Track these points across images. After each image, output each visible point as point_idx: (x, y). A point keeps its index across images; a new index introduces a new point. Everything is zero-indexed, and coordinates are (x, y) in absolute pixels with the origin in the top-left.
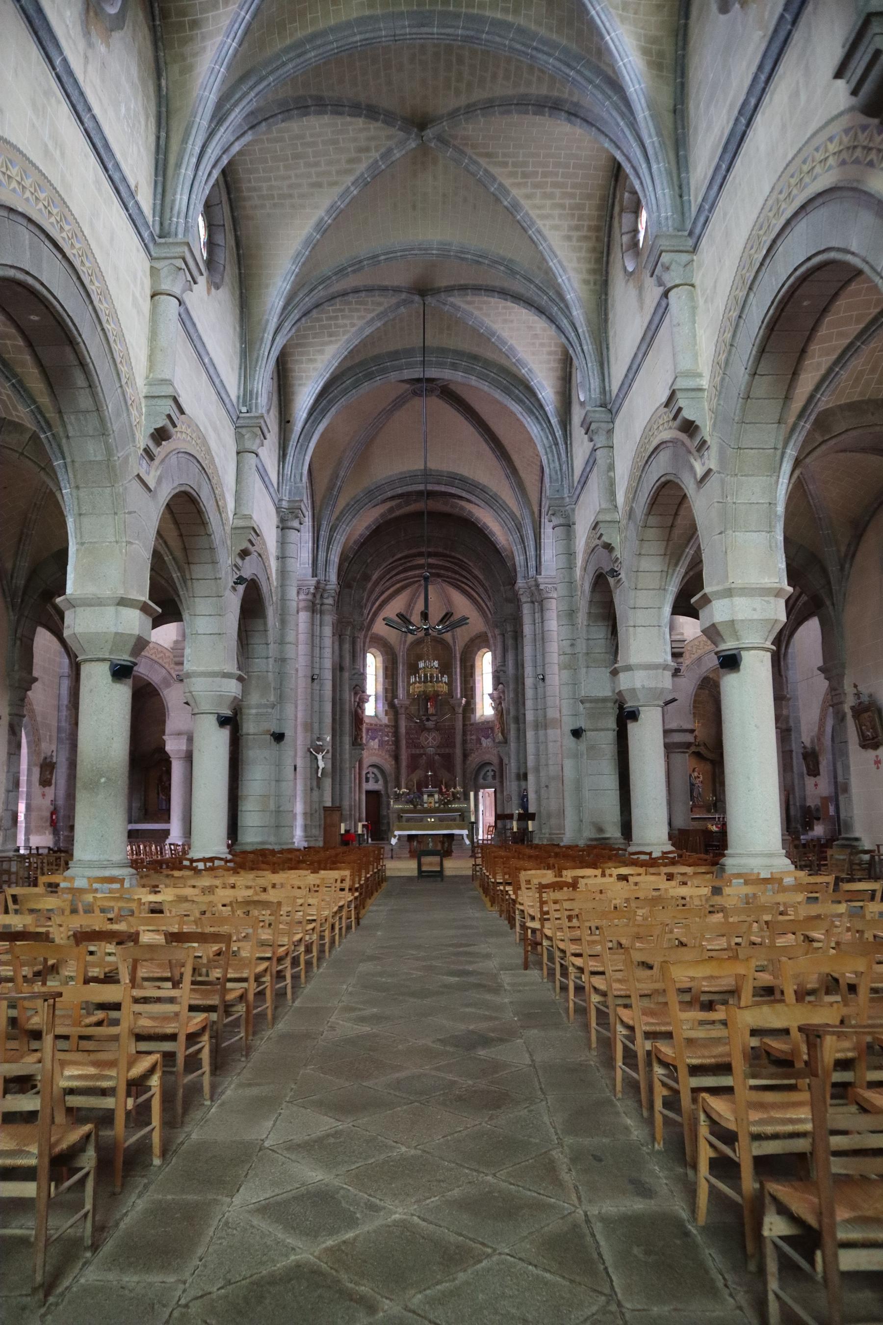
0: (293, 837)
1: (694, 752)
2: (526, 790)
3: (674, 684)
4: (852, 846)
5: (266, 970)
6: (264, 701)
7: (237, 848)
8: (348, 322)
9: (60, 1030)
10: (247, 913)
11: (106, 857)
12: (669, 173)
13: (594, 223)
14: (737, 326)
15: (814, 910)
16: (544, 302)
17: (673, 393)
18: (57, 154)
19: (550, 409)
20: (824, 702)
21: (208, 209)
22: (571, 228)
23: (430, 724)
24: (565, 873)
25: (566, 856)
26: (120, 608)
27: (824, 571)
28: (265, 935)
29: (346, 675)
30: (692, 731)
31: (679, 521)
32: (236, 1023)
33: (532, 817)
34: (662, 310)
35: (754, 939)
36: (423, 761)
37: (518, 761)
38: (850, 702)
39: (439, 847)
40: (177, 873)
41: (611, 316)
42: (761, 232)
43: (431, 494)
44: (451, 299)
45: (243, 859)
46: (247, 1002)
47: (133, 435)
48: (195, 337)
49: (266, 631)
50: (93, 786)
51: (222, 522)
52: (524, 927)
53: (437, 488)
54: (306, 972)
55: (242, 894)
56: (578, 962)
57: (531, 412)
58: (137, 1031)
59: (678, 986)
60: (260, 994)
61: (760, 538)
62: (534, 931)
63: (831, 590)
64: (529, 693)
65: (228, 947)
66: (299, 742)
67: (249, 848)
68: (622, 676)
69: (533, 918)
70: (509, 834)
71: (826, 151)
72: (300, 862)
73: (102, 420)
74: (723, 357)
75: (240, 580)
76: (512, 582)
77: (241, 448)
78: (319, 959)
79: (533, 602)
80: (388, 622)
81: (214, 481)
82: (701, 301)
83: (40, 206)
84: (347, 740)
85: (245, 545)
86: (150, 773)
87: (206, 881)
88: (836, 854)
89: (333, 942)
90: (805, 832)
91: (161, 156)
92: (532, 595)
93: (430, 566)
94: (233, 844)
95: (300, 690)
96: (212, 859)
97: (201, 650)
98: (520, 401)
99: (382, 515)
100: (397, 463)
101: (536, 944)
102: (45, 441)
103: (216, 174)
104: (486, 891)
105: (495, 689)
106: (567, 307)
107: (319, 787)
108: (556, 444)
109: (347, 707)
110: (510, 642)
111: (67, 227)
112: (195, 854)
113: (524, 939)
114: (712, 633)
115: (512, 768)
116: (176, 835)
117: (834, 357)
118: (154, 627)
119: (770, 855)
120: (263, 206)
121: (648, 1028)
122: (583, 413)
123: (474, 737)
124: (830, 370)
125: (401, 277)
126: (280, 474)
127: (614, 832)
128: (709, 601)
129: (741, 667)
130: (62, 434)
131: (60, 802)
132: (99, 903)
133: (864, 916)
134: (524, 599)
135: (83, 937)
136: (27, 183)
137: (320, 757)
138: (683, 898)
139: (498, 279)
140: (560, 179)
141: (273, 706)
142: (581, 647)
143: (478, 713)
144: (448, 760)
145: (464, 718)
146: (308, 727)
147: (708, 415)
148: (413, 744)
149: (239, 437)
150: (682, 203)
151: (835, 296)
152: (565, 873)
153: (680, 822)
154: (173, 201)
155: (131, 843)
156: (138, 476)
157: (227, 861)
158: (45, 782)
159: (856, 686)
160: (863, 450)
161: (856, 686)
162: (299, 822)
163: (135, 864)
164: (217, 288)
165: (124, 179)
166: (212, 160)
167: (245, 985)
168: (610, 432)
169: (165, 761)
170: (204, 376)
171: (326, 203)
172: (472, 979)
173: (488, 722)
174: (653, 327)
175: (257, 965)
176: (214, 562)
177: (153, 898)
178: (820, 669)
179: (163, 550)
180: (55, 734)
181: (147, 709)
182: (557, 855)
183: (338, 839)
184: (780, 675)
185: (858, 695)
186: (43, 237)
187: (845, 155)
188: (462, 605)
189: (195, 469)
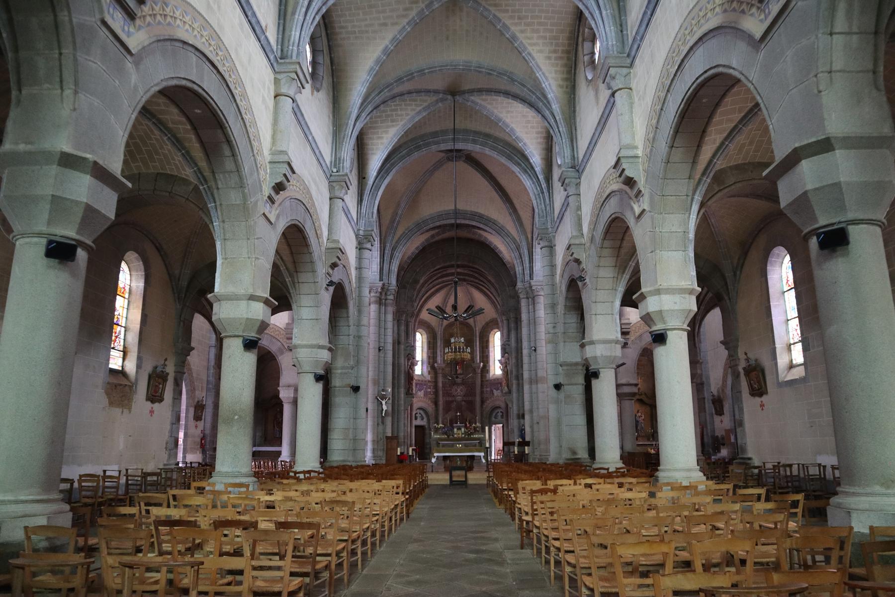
0: (365, 457)
1: (638, 400)
2: (524, 425)
3: (623, 354)
4: (746, 463)
5: (344, 548)
6: (346, 364)
7: (327, 464)
8: (404, 113)
9: (201, 588)
10: (332, 509)
11: (237, 469)
12: (614, 17)
13: (566, 48)
14: (660, 115)
15: (719, 508)
16: (533, 99)
17: (619, 159)
18: (215, 7)
19: (538, 169)
20: (726, 365)
21: (313, 41)
22: (550, 52)
23: (459, 381)
24: (549, 482)
25: (550, 471)
26: (250, 302)
27: (723, 277)
28: (344, 524)
29: (402, 347)
30: (636, 385)
31: (625, 244)
32: (322, 585)
33: (528, 444)
34: (611, 104)
35: (677, 528)
36: (454, 405)
37: (518, 406)
38: (742, 365)
39: (464, 465)
40: (285, 481)
41: (577, 108)
42: (674, 55)
43: (459, 226)
44: (472, 98)
45: (331, 471)
46: (330, 570)
47: (261, 187)
48: (303, 123)
49: (348, 317)
50: (229, 421)
51: (319, 244)
52: (521, 520)
53: (463, 222)
54: (372, 550)
55: (329, 496)
56: (557, 544)
57: (525, 171)
58: (255, 589)
59: (622, 560)
60: (340, 565)
61: (679, 255)
62: (528, 522)
63: (728, 289)
64: (526, 360)
65: (318, 531)
66: (370, 392)
67: (335, 464)
68: (587, 348)
69: (527, 514)
70: (512, 455)
71: (706, 8)
72: (369, 474)
73: (240, 177)
74: (651, 136)
75: (331, 283)
76: (514, 284)
77: (332, 196)
78: (380, 541)
79: (528, 298)
80: (430, 312)
81: (314, 217)
82: (636, 100)
83: (204, 40)
84: (402, 390)
85: (335, 260)
86: (268, 412)
87: (304, 487)
88: (735, 469)
89: (390, 529)
90: (715, 454)
91: (283, 7)
92: (527, 293)
93: (459, 274)
94: (324, 461)
95: (371, 357)
96: (309, 472)
97: (303, 330)
98: (518, 165)
99: (427, 240)
100: (436, 206)
101: (529, 531)
102: (203, 192)
103: (318, 18)
104: (496, 495)
105: (502, 357)
106: (548, 102)
107: (383, 423)
108: (543, 193)
109: (403, 368)
110: (512, 325)
111: (220, 53)
112: (298, 468)
113: (521, 527)
114: (647, 319)
115: (514, 410)
116: (285, 456)
117: (725, 135)
118: (272, 315)
119: (689, 470)
120: (349, 38)
121: (603, 590)
122: (560, 172)
124: (722, 144)
125: (439, 84)
126: (359, 212)
127: (583, 455)
128: (645, 298)
129: (668, 342)
130: (214, 186)
131: (208, 432)
132: (231, 501)
133: (752, 512)
134: (521, 296)
135: (220, 524)
136: (196, 25)
137: (384, 402)
138: (630, 500)
139: (503, 85)
140: (543, 20)
141: (352, 368)
142: (560, 328)
143: (491, 373)
144: (471, 406)
145: (482, 377)
146: (376, 382)
147: (642, 173)
148: (447, 394)
149: (331, 189)
150: (623, 36)
151: (724, 96)
152: (549, 482)
153: (629, 447)
154: (290, 36)
155: (255, 460)
156: (264, 214)
157: (319, 473)
158: (198, 418)
159: (746, 354)
160: (747, 196)
161: (746, 354)
162: (369, 447)
163: (257, 475)
164: (318, 91)
165: (258, 22)
166: (316, 9)
167: (329, 558)
168: (578, 185)
169: (279, 404)
170: (309, 148)
171: (390, 36)
172: (485, 556)
174: (605, 116)
175: (338, 545)
176: (314, 271)
177: (268, 498)
178: (721, 342)
179: (279, 263)
180: (205, 385)
181: (267, 368)
182: (544, 470)
183: (396, 458)
184: (695, 347)
185: (747, 360)
186: (204, 59)
187: (726, 6)
188: (481, 301)
189: (301, 209)
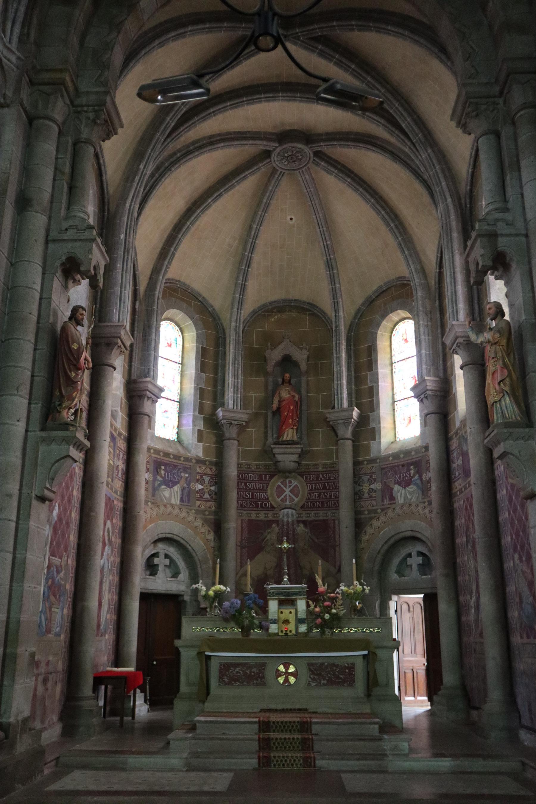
123: (377, 486)
143: (386, 438)
144: (322, 537)
145: (356, 450)
148: (252, 500)
173: (407, 453)
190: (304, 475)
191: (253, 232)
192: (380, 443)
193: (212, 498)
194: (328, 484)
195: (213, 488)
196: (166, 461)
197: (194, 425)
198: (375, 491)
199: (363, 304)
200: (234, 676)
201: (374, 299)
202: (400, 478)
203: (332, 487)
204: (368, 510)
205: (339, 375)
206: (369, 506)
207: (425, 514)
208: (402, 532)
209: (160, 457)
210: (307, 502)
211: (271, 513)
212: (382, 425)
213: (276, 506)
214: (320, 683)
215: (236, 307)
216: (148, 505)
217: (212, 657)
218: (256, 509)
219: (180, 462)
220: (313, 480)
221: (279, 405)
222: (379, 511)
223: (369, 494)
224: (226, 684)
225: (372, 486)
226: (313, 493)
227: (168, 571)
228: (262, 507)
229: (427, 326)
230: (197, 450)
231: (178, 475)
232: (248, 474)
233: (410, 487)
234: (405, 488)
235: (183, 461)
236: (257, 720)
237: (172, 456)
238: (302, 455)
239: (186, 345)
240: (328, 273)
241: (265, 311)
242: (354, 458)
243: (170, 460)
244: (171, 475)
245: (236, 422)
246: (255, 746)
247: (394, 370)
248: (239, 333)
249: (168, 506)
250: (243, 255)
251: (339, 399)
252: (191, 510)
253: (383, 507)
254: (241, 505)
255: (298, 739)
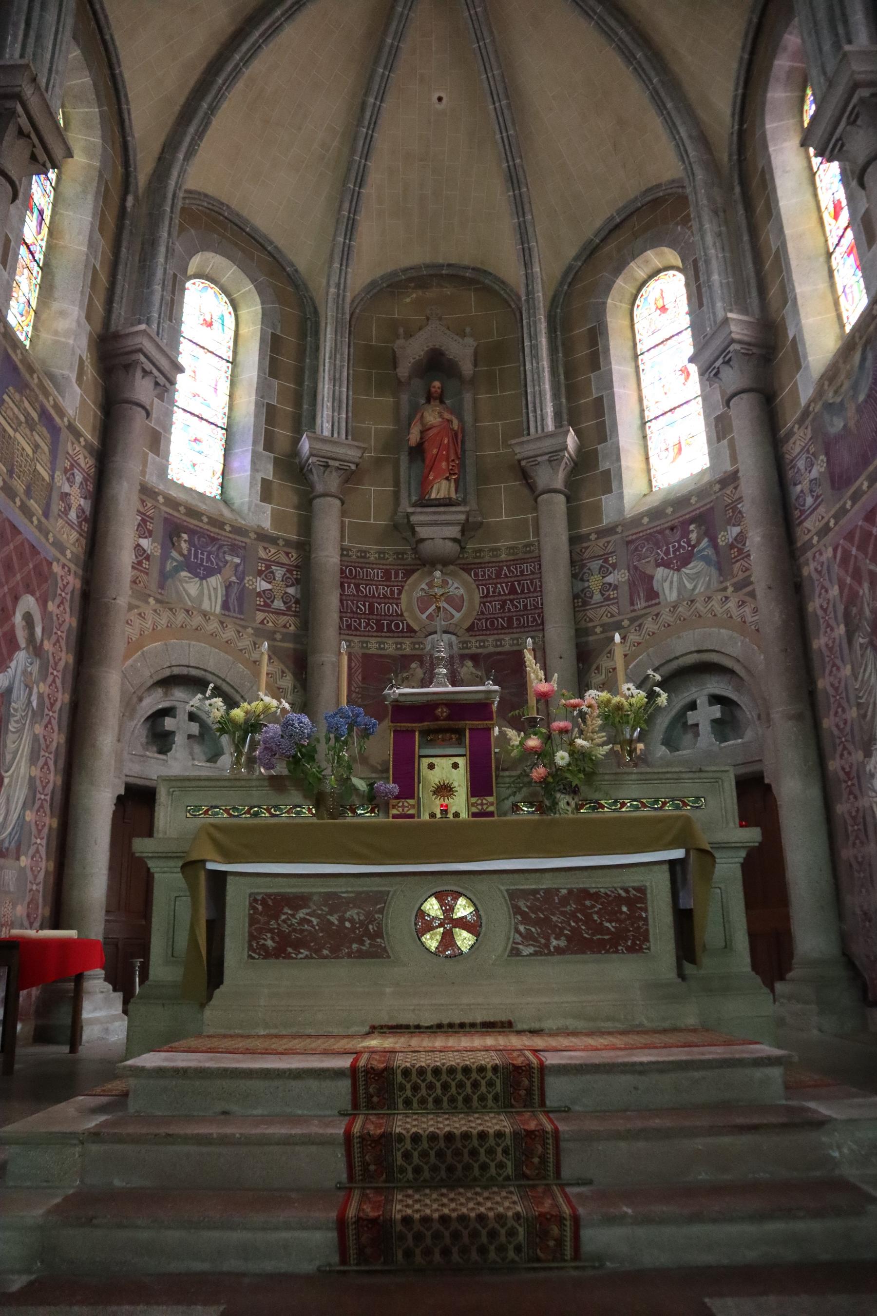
145: (573, 517)
148: (369, 615)
190: (472, 569)
191: (368, 114)
192: (621, 496)
193: (289, 608)
194: (519, 584)
195: (291, 590)
196: (192, 526)
197: (254, 468)
198: (616, 588)
199: (577, 258)
200: (295, 930)
201: (598, 245)
202: (667, 553)
203: (528, 588)
204: (602, 626)
205: (536, 376)
206: (604, 617)
207: (728, 611)
208: (677, 658)
209: (180, 515)
210: (479, 620)
211: (408, 641)
212: (624, 463)
213: (416, 628)
214: (547, 946)
215: (337, 260)
216: (148, 603)
217: (230, 879)
218: (379, 634)
219: (223, 533)
220: (490, 578)
221: (421, 438)
222: (626, 623)
223: (603, 595)
224: (267, 954)
225: (610, 579)
226: (490, 602)
227: (197, 749)
228: (389, 630)
229: (719, 234)
230: (263, 518)
231: (217, 556)
232: (361, 568)
233: (689, 566)
234: (678, 570)
235: (230, 532)
236: (345, 1063)
237: (205, 520)
238: (468, 528)
239: (243, 331)
240: (511, 193)
241: (393, 286)
242: (569, 530)
243: (201, 524)
244: (202, 554)
245: (337, 464)
246: (334, 1165)
247: (641, 367)
248: (343, 308)
249: (195, 613)
250: (350, 163)
251: (539, 417)
252: (245, 627)
253: (633, 614)
254: (349, 627)
255: (499, 1135)
